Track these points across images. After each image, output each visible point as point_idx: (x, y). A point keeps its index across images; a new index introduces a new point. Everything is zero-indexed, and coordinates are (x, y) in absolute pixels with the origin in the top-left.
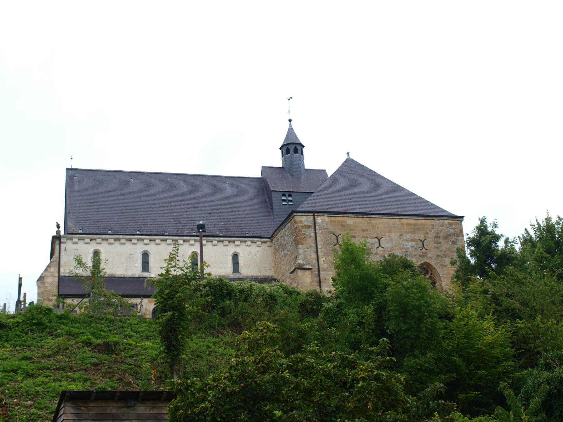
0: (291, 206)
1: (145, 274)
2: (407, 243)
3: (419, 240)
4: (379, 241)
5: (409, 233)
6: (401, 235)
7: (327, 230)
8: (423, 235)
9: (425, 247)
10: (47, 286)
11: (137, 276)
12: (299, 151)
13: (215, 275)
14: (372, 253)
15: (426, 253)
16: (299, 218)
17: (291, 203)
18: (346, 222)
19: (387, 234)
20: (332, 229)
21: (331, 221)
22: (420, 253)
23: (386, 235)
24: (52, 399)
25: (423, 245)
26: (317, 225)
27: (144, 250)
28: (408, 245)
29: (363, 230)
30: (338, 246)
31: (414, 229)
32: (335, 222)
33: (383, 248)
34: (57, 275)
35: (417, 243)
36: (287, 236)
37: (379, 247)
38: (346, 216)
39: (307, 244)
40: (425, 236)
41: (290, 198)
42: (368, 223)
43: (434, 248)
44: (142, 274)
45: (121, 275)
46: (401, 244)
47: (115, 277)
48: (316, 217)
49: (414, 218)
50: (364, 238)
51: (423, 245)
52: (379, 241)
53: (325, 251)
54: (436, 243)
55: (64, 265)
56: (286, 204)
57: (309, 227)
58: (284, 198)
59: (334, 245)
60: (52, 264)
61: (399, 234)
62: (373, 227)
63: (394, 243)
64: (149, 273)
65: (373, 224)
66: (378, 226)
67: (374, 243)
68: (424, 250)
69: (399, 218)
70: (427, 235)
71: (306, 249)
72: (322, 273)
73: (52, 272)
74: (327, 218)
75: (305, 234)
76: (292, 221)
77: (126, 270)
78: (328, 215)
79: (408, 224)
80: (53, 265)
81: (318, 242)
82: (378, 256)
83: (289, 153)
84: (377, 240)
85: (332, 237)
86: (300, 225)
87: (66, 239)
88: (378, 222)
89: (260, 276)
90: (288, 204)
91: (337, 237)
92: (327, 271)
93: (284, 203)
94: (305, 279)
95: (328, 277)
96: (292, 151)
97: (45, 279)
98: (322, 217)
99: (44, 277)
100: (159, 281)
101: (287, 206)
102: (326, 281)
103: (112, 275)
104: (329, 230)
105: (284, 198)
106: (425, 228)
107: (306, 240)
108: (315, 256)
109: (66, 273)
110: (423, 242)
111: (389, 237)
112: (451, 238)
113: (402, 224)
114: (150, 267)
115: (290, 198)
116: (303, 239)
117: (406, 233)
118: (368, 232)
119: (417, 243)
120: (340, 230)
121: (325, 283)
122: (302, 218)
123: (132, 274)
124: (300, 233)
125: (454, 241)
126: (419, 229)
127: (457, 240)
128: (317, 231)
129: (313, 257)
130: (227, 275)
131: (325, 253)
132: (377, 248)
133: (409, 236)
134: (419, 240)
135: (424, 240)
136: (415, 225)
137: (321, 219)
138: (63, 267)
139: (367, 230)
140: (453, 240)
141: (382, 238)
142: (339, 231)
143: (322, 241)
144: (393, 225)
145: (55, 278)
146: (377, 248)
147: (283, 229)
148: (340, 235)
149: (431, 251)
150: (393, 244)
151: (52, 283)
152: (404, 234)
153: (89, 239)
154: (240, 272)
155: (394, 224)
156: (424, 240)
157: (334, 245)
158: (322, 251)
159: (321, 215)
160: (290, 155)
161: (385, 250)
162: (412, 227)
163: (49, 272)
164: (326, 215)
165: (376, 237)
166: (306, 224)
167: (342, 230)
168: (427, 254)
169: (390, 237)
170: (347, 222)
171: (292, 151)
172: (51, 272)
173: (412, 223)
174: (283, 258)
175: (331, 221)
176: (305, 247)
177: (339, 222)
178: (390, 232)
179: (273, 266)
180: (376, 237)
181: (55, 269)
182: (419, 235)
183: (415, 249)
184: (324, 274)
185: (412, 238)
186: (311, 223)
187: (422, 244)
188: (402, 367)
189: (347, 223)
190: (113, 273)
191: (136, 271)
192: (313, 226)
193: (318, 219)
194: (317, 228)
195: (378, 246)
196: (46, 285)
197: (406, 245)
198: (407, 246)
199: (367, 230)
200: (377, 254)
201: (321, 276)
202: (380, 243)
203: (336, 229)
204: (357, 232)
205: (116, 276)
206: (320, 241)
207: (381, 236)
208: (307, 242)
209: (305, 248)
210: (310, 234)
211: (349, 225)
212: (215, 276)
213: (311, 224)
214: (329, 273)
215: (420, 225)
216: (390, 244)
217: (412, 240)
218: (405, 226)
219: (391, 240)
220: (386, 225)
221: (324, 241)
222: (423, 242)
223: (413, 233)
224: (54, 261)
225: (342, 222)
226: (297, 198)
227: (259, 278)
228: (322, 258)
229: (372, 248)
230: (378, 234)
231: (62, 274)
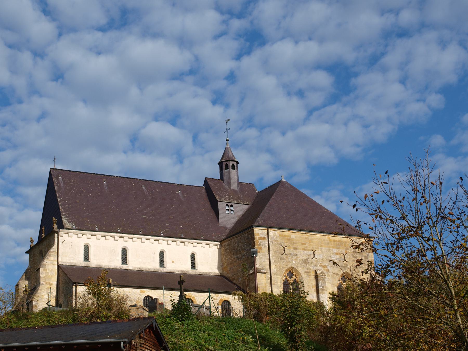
0: (232, 215)
1: (125, 267)
2: (333, 256)
3: (342, 254)
4: (314, 253)
5: (335, 248)
6: (329, 249)
7: (277, 242)
8: (345, 250)
9: (346, 260)
10: (48, 272)
11: (119, 268)
13: (178, 270)
14: (309, 262)
15: (347, 265)
16: (257, 231)
17: (232, 212)
18: (290, 237)
19: (320, 247)
20: (280, 241)
21: (280, 235)
22: (342, 265)
23: (319, 249)
25: (345, 258)
26: (270, 237)
27: (124, 246)
28: (334, 257)
29: (303, 244)
30: (284, 255)
31: (338, 245)
33: (317, 259)
34: (56, 263)
35: (341, 256)
37: (313, 258)
38: (290, 231)
39: (262, 252)
40: (346, 251)
41: (232, 208)
42: (306, 238)
43: (352, 260)
44: (122, 266)
45: (106, 266)
46: (329, 256)
47: (101, 268)
48: (269, 231)
49: (339, 236)
50: (303, 250)
51: (345, 258)
52: (314, 253)
53: (275, 259)
54: (353, 257)
55: (62, 255)
56: (229, 213)
57: (264, 238)
58: (227, 208)
59: (282, 255)
60: (52, 253)
61: (328, 248)
62: (310, 242)
63: (324, 255)
64: (127, 265)
65: (310, 240)
66: (313, 241)
68: (345, 262)
69: (328, 235)
70: (347, 250)
71: (261, 256)
72: (272, 276)
73: (53, 261)
74: (277, 232)
75: (261, 244)
77: (110, 262)
78: (278, 230)
79: (334, 241)
80: (52, 254)
81: (270, 251)
82: (313, 265)
84: (312, 252)
85: (280, 247)
86: (257, 237)
87: (63, 233)
88: (313, 238)
89: (212, 273)
90: (230, 213)
91: (284, 248)
92: (277, 275)
93: (227, 212)
94: (262, 281)
95: (277, 280)
97: (46, 266)
98: (274, 231)
99: (46, 264)
101: (230, 214)
102: (276, 283)
103: (99, 265)
104: (278, 242)
105: (227, 208)
106: (346, 244)
107: (262, 249)
108: (268, 263)
109: (63, 262)
110: (344, 256)
111: (320, 250)
112: (364, 254)
113: (330, 241)
114: (128, 260)
115: (232, 208)
116: (260, 248)
117: (333, 247)
118: (306, 246)
119: (341, 256)
120: (286, 242)
121: (275, 284)
122: (259, 231)
123: (115, 266)
124: (258, 244)
125: (366, 256)
126: (342, 245)
128: (270, 243)
129: (267, 263)
130: (187, 270)
131: (275, 261)
132: (312, 259)
133: (335, 251)
134: (342, 254)
135: (346, 254)
136: (339, 241)
137: (273, 233)
138: (61, 257)
140: (366, 255)
141: (316, 251)
142: (285, 243)
143: (273, 251)
144: (324, 241)
145: (54, 266)
146: (312, 259)
147: (238, 237)
148: (286, 246)
149: (350, 263)
150: (323, 256)
151: (52, 270)
152: (331, 249)
153: (82, 234)
154: (196, 268)
155: (324, 240)
156: (346, 254)
157: (282, 255)
158: (273, 259)
159: (273, 229)
160: (228, 170)
161: (318, 261)
162: (337, 243)
163: (50, 260)
164: (276, 230)
165: (311, 250)
166: (262, 236)
167: (288, 243)
168: (347, 265)
169: (321, 250)
170: (291, 237)
172: (51, 261)
173: (337, 240)
175: (280, 235)
176: (261, 255)
177: (285, 236)
178: (322, 246)
179: (221, 265)
180: (311, 250)
181: (54, 258)
182: (342, 250)
183: (339, 261)
184: (274, 277)
185: (337, 252)
186: (266, 236)
187: (344, 258)
188: (13, 314)
189: (291, 238)
190: (100, 264)
191: (116, 263)
192: (267, 238)
193: (270, 232)
194: (270, 240)
195: (313, 257)
196: (47, 271)
197: (333, 258)
198: (334, 258)
201: (272, 279)
202: (314, 255)
203: (284, 241)
204: (298, 245)
205: (102, 267)
206: (272, 251)
207: (315, 249)
208: (262, 250)
209: (261, 256)
210: (264, 244)
211: (292, 239)
213: (265, 237)
214: (278, 276)
215: (343, 242)
216: (322, 256)
217: (337, 254)
218: (332, 242)
219: (322, 253)
220: (319, 241)
221: (274, 251)
222: (344, 256)
224: (53, 251)
226: (237, 208)
227: (211, 274)
228: (273, 264)
229: (309, 258)
230: (313, 248)
231: (60, 263)
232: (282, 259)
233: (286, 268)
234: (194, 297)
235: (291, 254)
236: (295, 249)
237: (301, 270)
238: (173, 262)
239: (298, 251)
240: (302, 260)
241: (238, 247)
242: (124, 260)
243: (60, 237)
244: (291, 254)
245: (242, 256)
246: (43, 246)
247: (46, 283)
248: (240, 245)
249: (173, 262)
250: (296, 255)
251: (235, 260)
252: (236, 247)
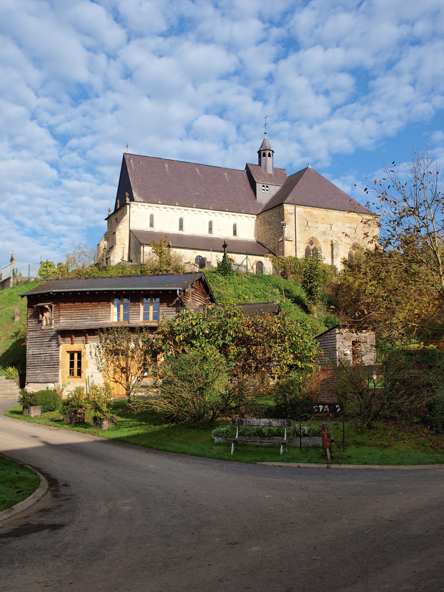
0: (267, 194)
6: (344, 224)
12: (271, 156)
17: (267, 192)
18: (313, 213)
19: (336, 222)
21: (305, 211)
24: (347, 277)
29: (322, 219)
32: (306, 212)
36: (274, 217)
40: (357, 226)
41: (267, 189)
42: (326, 215)
57: (292, 214)
67: (328, 228)
72: (297, 243)
76: (281, 208)
79: (348, 217)
83: (265, 156)
91: (308, 222)
92: (301, 243)
93: (263, 191)
96: (267, 155)
100: (116, 227)
101: (265, 194)
105: (263, 188)
113: (345, 217)
115: (267, 189)
117: (347, 222)
127: (374, 229)
131: (300, 232)
133: (348, 225)
139: (324, 219)
162: (350, 219)
169: (337, 224)
171: (267, 155)
174: (268, 230)
177: (309, 212)
178: (337, 221)
199: (324, 219)
200: (329, 234)
212: (240, 238)
217: (350, 228)
218: (346, 218)
219: (338, 227)
223: (351, 223)
225: (310, 212)
230: (330, 222)
232: (305, 230)
233: (308, 237)
234: (234, 258)
235: (312, 227)
236: (316, 222)
237: (320, 240)
238: (219, 230)
239: (318, 224)
240: (322, 232)
241: (271, 219)
242: (181, 227)
243: (131, 208)
244: (312, 227)
245: (274, 227)
246: (118, 215)
247: (121, 244)
248: (273, 218)
249: (219, 230)
250: (317, 228)
251: (268, 230)
252: (270, 220)
